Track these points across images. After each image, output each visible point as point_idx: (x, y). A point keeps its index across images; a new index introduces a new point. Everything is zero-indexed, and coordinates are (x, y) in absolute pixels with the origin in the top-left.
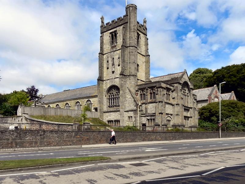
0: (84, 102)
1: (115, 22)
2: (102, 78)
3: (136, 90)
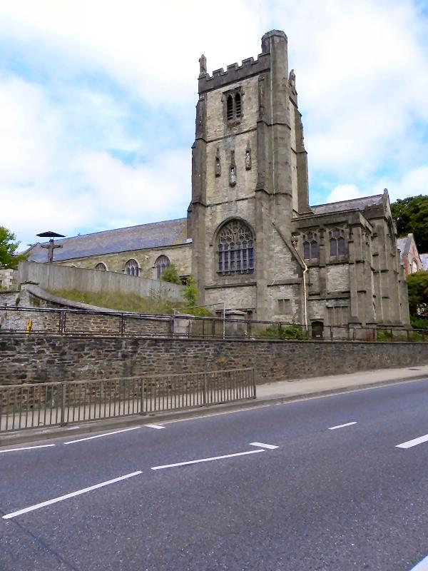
0: (149, 262)
1: (236, 69)
2: (203, 200)
3: (294, 231)
